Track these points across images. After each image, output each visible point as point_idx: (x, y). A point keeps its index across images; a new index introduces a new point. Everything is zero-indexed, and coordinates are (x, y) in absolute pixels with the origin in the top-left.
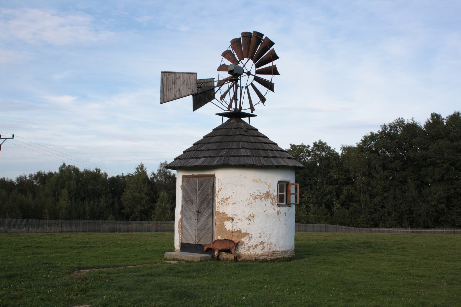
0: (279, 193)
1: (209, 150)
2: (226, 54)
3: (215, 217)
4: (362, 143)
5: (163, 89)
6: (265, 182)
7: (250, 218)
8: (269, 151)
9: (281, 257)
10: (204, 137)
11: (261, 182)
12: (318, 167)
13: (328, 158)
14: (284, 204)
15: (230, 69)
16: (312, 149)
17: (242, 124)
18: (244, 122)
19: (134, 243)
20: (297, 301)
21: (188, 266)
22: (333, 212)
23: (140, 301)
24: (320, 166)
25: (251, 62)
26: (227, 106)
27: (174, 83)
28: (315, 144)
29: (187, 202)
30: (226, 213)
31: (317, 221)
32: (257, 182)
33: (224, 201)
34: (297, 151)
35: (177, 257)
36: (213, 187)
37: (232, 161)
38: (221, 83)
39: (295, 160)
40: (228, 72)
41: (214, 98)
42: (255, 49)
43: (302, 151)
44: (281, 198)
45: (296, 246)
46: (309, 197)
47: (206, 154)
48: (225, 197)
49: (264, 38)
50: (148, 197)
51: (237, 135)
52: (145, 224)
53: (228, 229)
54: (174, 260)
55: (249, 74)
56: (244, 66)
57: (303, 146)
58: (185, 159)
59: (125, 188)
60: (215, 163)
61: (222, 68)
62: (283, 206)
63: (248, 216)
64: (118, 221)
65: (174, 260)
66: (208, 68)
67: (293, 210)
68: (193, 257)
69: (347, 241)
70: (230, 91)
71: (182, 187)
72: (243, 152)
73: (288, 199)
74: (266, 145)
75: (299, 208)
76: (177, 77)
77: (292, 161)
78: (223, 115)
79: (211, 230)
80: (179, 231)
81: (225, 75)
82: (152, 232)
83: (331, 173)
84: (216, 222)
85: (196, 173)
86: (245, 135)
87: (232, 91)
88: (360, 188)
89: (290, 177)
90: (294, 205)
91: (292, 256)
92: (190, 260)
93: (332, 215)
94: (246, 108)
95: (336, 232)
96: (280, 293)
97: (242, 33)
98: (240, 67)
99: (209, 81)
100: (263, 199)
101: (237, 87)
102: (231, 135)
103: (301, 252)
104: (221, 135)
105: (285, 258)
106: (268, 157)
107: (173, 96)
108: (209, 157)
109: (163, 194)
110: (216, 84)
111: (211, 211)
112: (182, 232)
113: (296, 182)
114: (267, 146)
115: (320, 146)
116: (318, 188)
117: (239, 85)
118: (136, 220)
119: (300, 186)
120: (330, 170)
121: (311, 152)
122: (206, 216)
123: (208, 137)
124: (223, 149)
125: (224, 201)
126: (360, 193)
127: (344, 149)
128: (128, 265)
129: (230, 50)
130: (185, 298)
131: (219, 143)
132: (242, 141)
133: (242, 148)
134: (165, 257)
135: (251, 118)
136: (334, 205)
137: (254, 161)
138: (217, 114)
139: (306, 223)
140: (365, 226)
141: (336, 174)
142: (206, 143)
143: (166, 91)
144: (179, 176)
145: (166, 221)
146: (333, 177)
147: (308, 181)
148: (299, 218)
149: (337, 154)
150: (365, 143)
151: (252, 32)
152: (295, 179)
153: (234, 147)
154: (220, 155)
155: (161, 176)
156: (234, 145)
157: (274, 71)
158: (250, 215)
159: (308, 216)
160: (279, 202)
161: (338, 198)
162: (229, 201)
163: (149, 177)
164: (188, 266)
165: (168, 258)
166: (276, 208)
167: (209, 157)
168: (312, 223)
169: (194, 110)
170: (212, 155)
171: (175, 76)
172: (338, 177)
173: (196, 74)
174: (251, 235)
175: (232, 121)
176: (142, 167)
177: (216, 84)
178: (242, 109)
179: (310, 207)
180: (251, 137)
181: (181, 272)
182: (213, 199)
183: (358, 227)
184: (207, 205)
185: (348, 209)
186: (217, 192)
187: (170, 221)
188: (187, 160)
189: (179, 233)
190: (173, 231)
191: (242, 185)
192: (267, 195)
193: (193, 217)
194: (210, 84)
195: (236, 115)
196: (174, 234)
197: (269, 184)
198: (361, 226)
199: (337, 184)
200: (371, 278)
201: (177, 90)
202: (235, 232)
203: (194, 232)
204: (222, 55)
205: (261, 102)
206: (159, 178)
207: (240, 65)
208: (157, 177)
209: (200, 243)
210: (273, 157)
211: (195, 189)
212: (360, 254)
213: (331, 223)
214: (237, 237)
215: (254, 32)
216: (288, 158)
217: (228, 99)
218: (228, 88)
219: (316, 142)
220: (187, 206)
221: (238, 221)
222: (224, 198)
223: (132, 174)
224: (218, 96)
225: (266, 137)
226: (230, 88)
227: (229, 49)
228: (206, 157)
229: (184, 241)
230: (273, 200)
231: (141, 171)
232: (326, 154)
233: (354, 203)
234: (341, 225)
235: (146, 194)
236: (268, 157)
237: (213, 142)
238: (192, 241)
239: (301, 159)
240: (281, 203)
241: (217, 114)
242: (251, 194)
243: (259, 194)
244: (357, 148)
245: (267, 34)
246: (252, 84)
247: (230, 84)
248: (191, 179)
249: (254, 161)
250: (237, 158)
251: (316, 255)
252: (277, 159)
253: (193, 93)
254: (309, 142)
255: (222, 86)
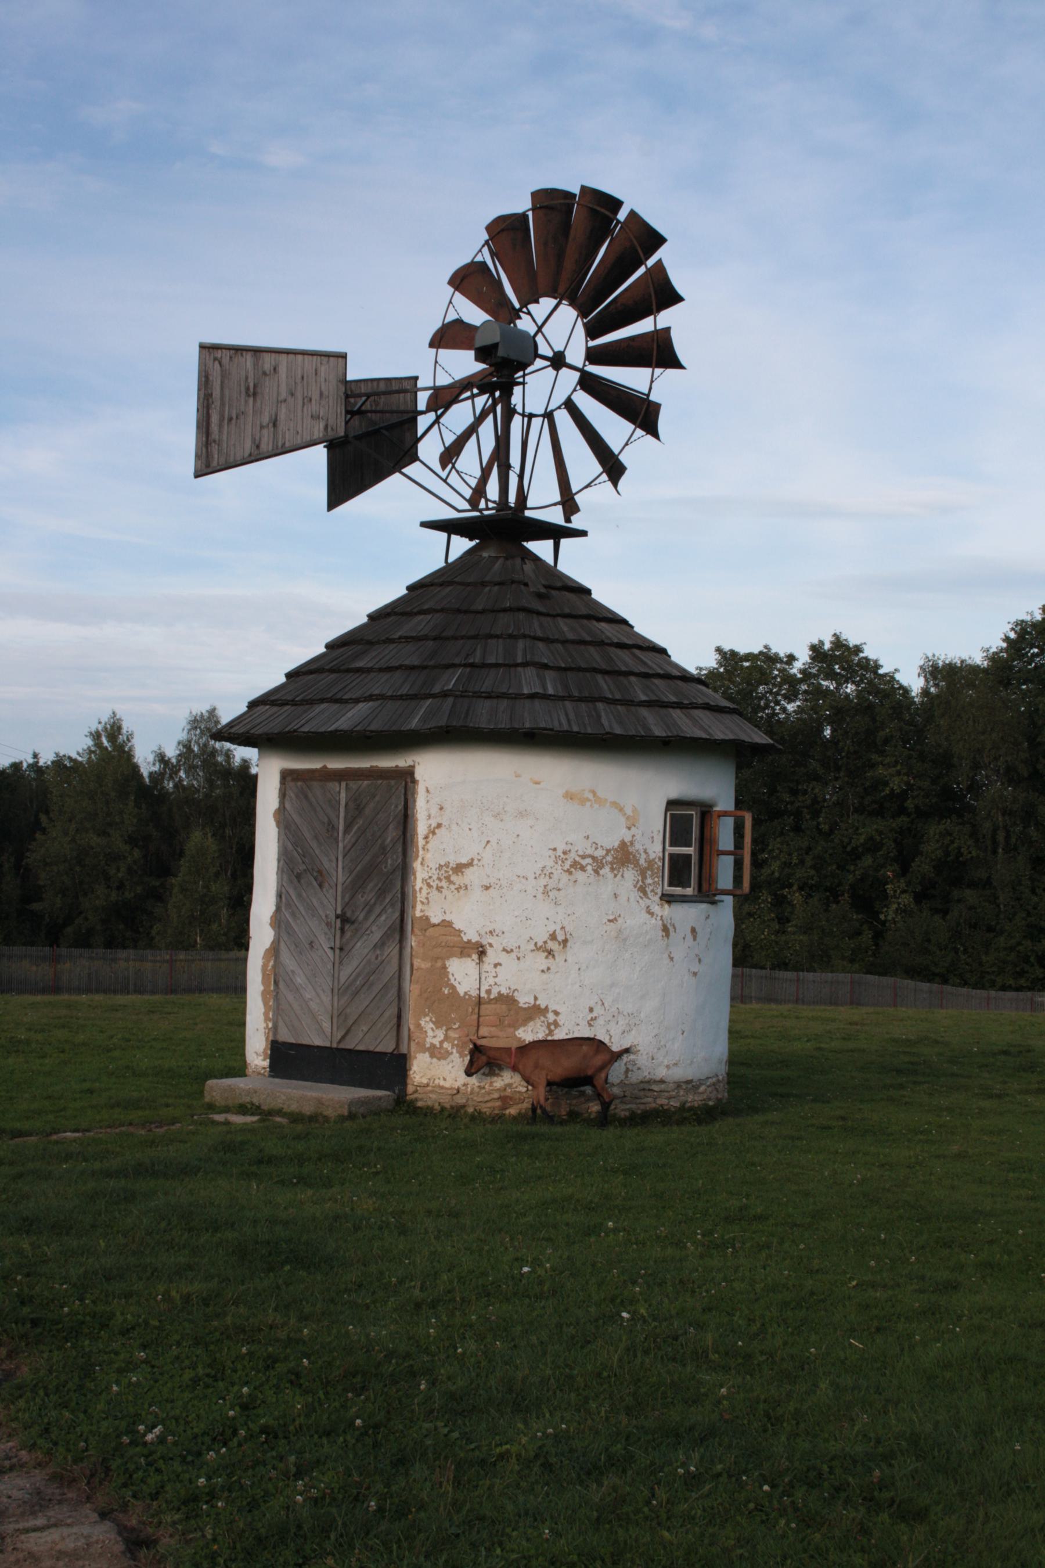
0: (670, 849)
1: (389, 669)
2: (469, 280)
3: (412, 941)
4: (1006, 650)
5: (208, 416)
6: (615, 804)
7: (551, 945)
8: (633, 679)
9: (675, 1103)
10: (372, 617)
11: (599, 801)
12: (826, 744)
13: (870, 706)
14: (689, 891)
15: (480, 341)
16: (803, 671)
17: (528, 567)
18: (536, 559)
19: (81, 1038)
20: (735, 1285)
21: (298, 1137)
22: (883, 923)
23: (108, 1279)
24: (834, 741)
25: (567, 313)
26: (468, 493)
27: (253, 393)
28: (816, 650)
29: (298, 877)
30: (458, 925)
31: (819, 958)
32: (583, 801)
33: (448, 878)
34: (746, 677)
35: (255, 1101)
36: (406, 819)
37: (483, 714)
38: (444, 399)
39: (736, 717)
40: (471, 354)
41: (414, 458)
42: (585, 261)
43: (765, 678)
44: (678, 870)
45: (734, 1060)
46: (787, 865)
47: (380, 684)
48: (454, 860)
49: (622, 216)
50: (137, 853)
51: (505, 610)
52: (126, 962)
53: (461, 990)
54: (243, 1109)
55: (558, 361)
56: (540, 329)
57: (768, 658)
58: (293, 703)
59: (47, 812)
60: (414, 723)
61: (450, 335)
62: (683, 899)
63: (546, 937)
64: (17, 950)
65: (243, 1109)
66: (392, 328)
67: (724, 915)
68: (320, 1101)
69: (936, 1042)
70: (481, 429)
71: (282, 816)
72: (529, 681)
73: (705, 875)
74: (624, 654)
75: (747, 908)
76: (267, 367)
77: (727, 718)
78: (448, 527)
79: (393, 991)
80: (264, 994)
81: (463, 363)
82: (153, 992)
83: (880, 770)
84: (417, 962)
85: (336, 764)
86: (539, 613)
87: (487, 431)
88: (995, 830)
89: (715, 786)
90: (729, 900)
91: (719, 1100)
92: (308, 1109)
93: (878, 935)
94: (542, 501)
95: (895, 1005)
96: (669, 1251)
97: (536, 195)
98: (524, 334)
99: (395, 387)
100: (606, 871)
101: (510, 412)
102: (483, 612)
103: (754, 1082)
104: (442, 610)
105: (691, 1109)
106: (629, 703)
107: (248, 444)
108: (392, 698)
109: (199, 840)
110: (423, 399)
111: (397, 914)
112: (277, 998)
113: (739, 804)
114: (624, 660)
115: (838, 658)
116: (825, 828)
117: (519, 409)
118: (88, 946)
119: (754, 819)
120: (875, 757)
121: (801, 681)
122: (377, 936)
123: (388, 615)
124: (448, 666)
125: (448, 878)
126: (995, 852)
127: (934, 671)
128: (56, 1131)
129: (484, 264)
130: (287, 1268)
131: (430, 643)
132: (525, 636)
133: (525, 665)
134: (207, 1099)
135: (564, 542)
136: (886, 897)
137: (572, 716)
138: (425, 525)
139: (773, 968)
140: (1011, 982)
141: (899, 773)
142: (378, 642)
143: (220, 426)
144: (269, 773)
145: (212, 949)
146: (886, 784)
147: (787, 797)
148: (746, 946)
149: (906, 691)
150: (1019, 650)
151: (576, 190)
152: (736, 791)
153: (491, 660)
154: (437, 689)
155: (191, 769)
156: (496, 652)
157: (659, 353)
158: (553, 937)
159: (783, 938)
160: (670, 885)
161: (905, 870)
162: (471, 876)
163: (145, 772)
164: (298, 1137)
165: (220, 1102)
166: (656, 909)
167: (392, 698)
168: (798, 968)
169: (332, 504)
170: (404, 690)
171: (256, 365)
172: (908, 784)
173: (344, 356)
174: (556, 1013)
175: (485, 554)
176: (114, 730)
177: (423, 399)
178: (530, 503)
179: (790, 903)
180: (561, 622)
181: (270, 1160)
182: (404, 870)
183: (983, 988)
184: (382, 893)
185: (945, 912)
186: (421, 842)
187: (228, 950)
188: (301, 708)
189: (265, 1003)
190: (241, 989)
191: (522, 814)
192: (624, 856)
193: (322, 939)
194: (399, 401)
195: (501, 530)
196: (244, 1003)
197: (629, 811)
198: (993, 985)
199: (902, 811)
200: (1033, 1198)
201: (266, 419)
202: (490, 1001)
203: (326, 999)
204: (451, 282)
205: (605, 477)
206: (182, 774)
207: (525, 324)
208: (174, 770)
209: (350, 1044)
210: (649, 704)
211: (332, 827)
212: (991, 1097)
213: (870, 970)
214: (500, 1023)
215: (583, 189)
216: (707, 707)
217: (469, 462)
218: (470, 420)
219: (821, 643)
220: (299, 896)
221: (503, 958)
222: (447, 865)
223: (74, 756)
224: (430, 449)
225: (624, 622)
226: (479, 420)
227: (479, 258)
228: (381, 697)
229: (286, 1036)
230: (644, 878)
231: (112, 744)
232: (859, 694)
233: (968, 892)
234: (912, 978)
235: (132, 840)
236: (629, 703)
237: (408, 639)
238: (317, 1032)
239: (758, 708)
240: (678, 890)
241: (425, 525)
242: (559, 853)
243: (589, 852)
244: (985, 671)
245: (638, 199)
246: (569, 405)
247: (481, 401)
248: (315, 784)
249: (572, 716)
250: (504, 703)
251: (814, 1101)
252: (663, 711)
253: (331, 435)
254: (794, 642)
255: (447, 408)
